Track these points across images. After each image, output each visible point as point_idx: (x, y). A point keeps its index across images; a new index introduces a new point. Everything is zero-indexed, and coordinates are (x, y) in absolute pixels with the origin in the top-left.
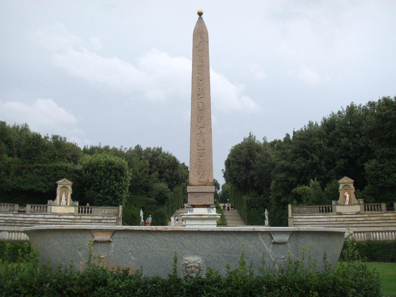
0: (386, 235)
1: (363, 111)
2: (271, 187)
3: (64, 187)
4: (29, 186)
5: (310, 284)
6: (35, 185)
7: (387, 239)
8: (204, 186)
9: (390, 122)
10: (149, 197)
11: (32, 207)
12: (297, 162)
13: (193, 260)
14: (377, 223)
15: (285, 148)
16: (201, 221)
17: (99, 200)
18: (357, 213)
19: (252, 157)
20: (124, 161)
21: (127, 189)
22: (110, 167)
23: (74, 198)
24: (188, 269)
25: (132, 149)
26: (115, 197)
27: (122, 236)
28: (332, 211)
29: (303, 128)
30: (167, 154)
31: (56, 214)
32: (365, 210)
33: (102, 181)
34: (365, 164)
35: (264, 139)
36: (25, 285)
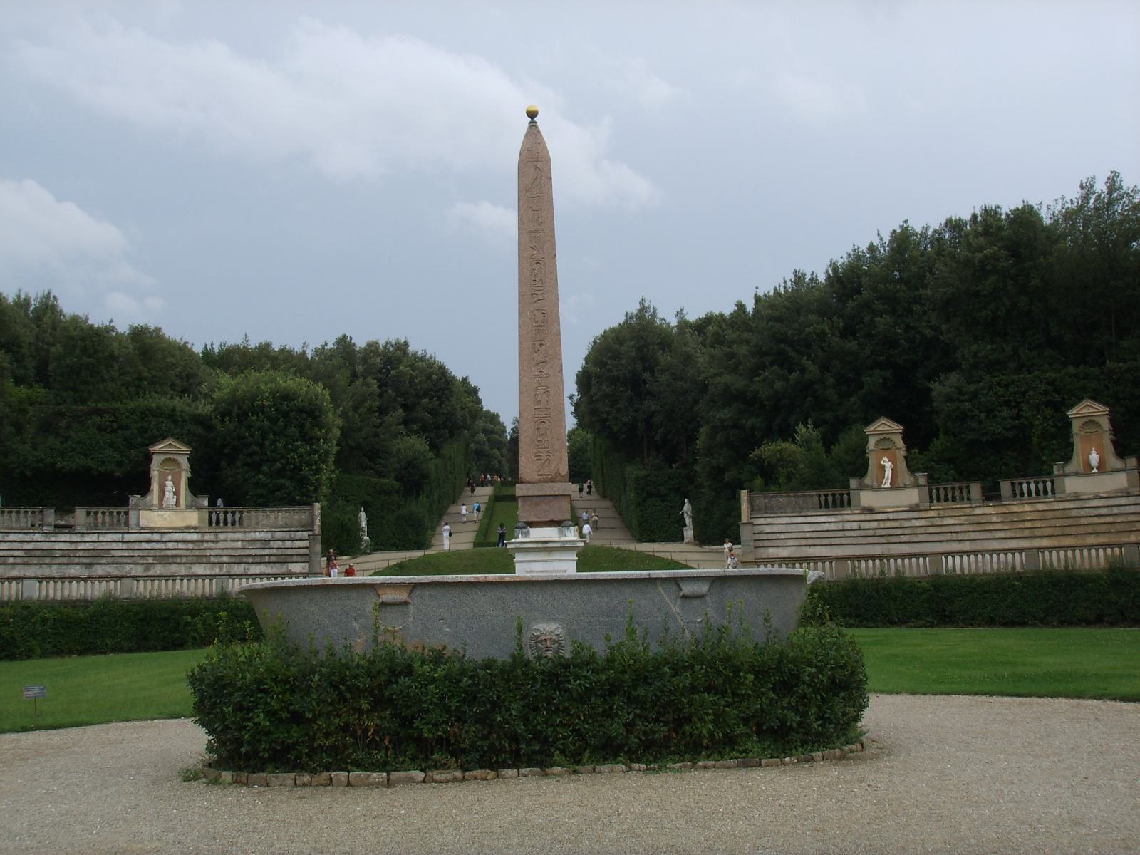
0: (976, 562)
1: (932, 243)
2: (699, 445)
3: (170, 461)
4: (77, 460)
5: (742, 663)
6: (93, 458)
7: (981, 571)
8: (550, 484)
9: (994, 278)
10: (381, 475)
11: (88, 514)
12: (764, 380)
13: (547, 628)
14: (957, 532)
15: (733, 342)
16: (546, 553)
17: (260, 491)
18: (912, 509)
19: (647, 365)
20: (319, 388)
21: (332, 459)
22: (285, 406)
23: (195, 487)
25: (328, 347)
26: (302, 482)
27: (428, 593)
28: (849, 504)
29: (780, 286)
30: (423, 359)
31: (152, 530)
32: (931, 501)
33: (267, 443)
34: (932, 385)
35: (680, 314)
36: (275, 680)
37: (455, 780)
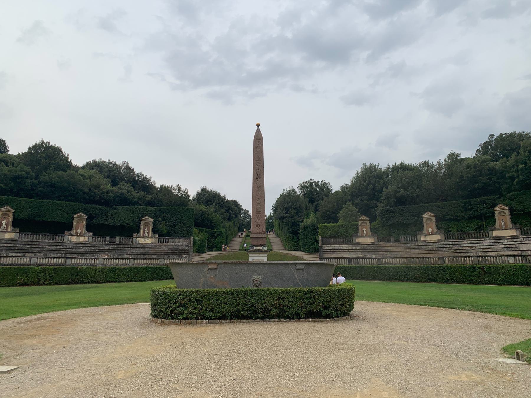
37: (228, 323)
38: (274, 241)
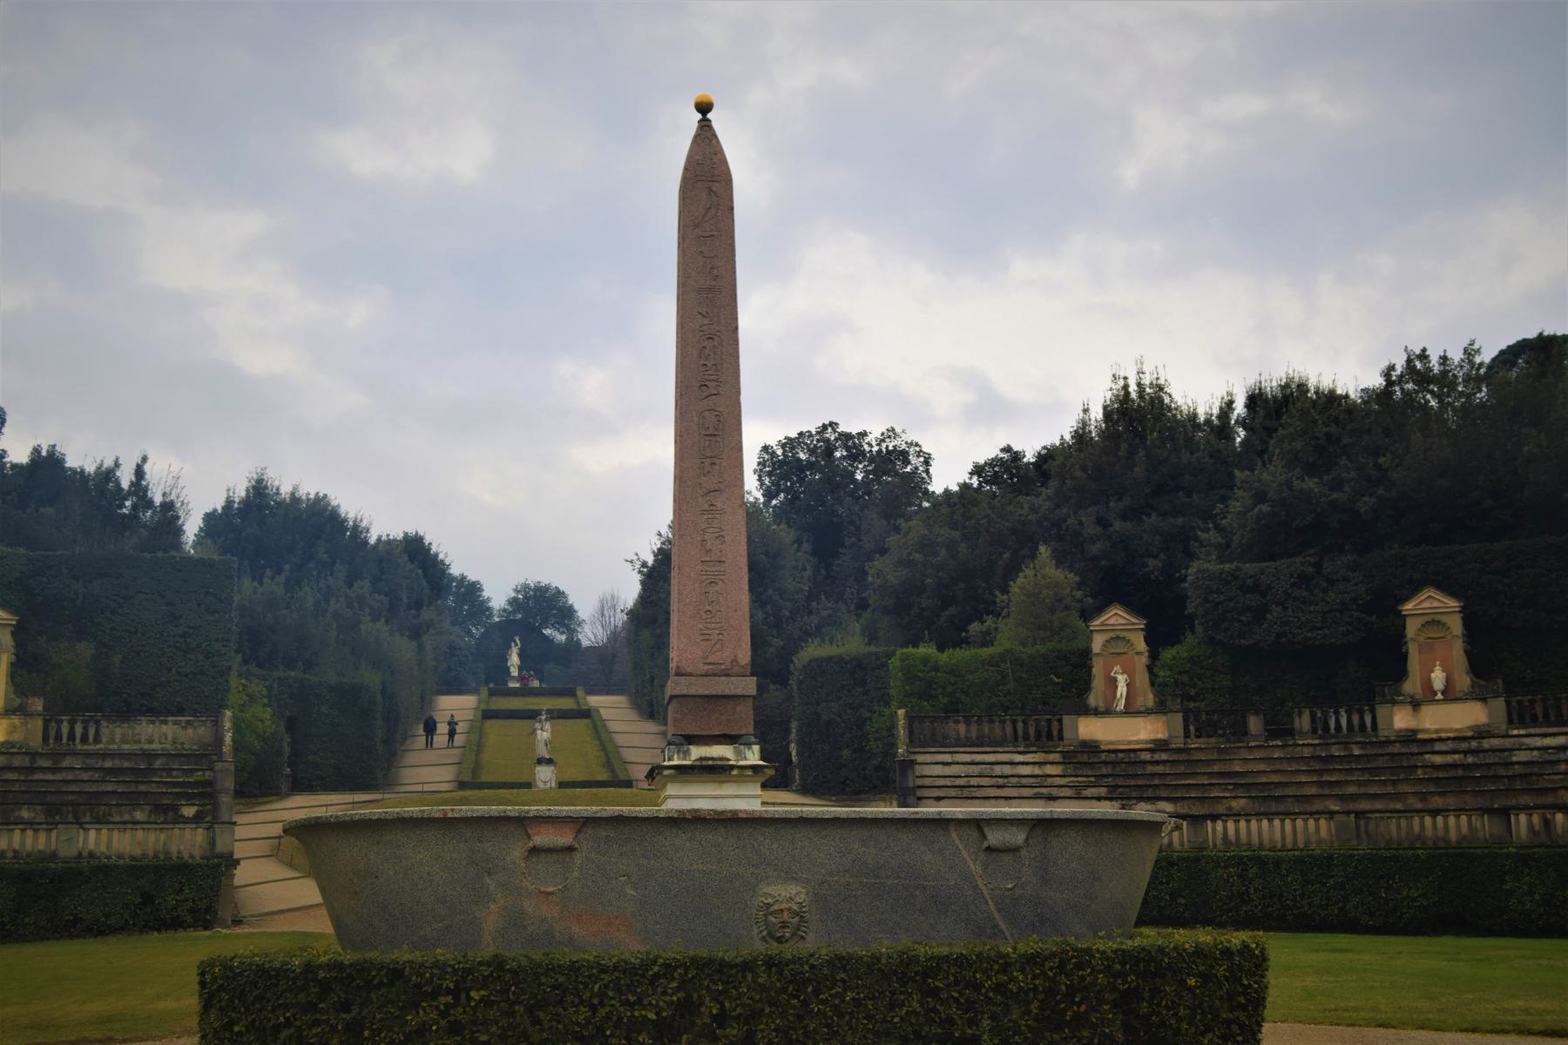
24: (771, 918)
38: (637, 740)
